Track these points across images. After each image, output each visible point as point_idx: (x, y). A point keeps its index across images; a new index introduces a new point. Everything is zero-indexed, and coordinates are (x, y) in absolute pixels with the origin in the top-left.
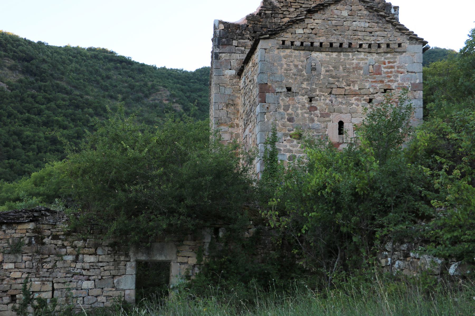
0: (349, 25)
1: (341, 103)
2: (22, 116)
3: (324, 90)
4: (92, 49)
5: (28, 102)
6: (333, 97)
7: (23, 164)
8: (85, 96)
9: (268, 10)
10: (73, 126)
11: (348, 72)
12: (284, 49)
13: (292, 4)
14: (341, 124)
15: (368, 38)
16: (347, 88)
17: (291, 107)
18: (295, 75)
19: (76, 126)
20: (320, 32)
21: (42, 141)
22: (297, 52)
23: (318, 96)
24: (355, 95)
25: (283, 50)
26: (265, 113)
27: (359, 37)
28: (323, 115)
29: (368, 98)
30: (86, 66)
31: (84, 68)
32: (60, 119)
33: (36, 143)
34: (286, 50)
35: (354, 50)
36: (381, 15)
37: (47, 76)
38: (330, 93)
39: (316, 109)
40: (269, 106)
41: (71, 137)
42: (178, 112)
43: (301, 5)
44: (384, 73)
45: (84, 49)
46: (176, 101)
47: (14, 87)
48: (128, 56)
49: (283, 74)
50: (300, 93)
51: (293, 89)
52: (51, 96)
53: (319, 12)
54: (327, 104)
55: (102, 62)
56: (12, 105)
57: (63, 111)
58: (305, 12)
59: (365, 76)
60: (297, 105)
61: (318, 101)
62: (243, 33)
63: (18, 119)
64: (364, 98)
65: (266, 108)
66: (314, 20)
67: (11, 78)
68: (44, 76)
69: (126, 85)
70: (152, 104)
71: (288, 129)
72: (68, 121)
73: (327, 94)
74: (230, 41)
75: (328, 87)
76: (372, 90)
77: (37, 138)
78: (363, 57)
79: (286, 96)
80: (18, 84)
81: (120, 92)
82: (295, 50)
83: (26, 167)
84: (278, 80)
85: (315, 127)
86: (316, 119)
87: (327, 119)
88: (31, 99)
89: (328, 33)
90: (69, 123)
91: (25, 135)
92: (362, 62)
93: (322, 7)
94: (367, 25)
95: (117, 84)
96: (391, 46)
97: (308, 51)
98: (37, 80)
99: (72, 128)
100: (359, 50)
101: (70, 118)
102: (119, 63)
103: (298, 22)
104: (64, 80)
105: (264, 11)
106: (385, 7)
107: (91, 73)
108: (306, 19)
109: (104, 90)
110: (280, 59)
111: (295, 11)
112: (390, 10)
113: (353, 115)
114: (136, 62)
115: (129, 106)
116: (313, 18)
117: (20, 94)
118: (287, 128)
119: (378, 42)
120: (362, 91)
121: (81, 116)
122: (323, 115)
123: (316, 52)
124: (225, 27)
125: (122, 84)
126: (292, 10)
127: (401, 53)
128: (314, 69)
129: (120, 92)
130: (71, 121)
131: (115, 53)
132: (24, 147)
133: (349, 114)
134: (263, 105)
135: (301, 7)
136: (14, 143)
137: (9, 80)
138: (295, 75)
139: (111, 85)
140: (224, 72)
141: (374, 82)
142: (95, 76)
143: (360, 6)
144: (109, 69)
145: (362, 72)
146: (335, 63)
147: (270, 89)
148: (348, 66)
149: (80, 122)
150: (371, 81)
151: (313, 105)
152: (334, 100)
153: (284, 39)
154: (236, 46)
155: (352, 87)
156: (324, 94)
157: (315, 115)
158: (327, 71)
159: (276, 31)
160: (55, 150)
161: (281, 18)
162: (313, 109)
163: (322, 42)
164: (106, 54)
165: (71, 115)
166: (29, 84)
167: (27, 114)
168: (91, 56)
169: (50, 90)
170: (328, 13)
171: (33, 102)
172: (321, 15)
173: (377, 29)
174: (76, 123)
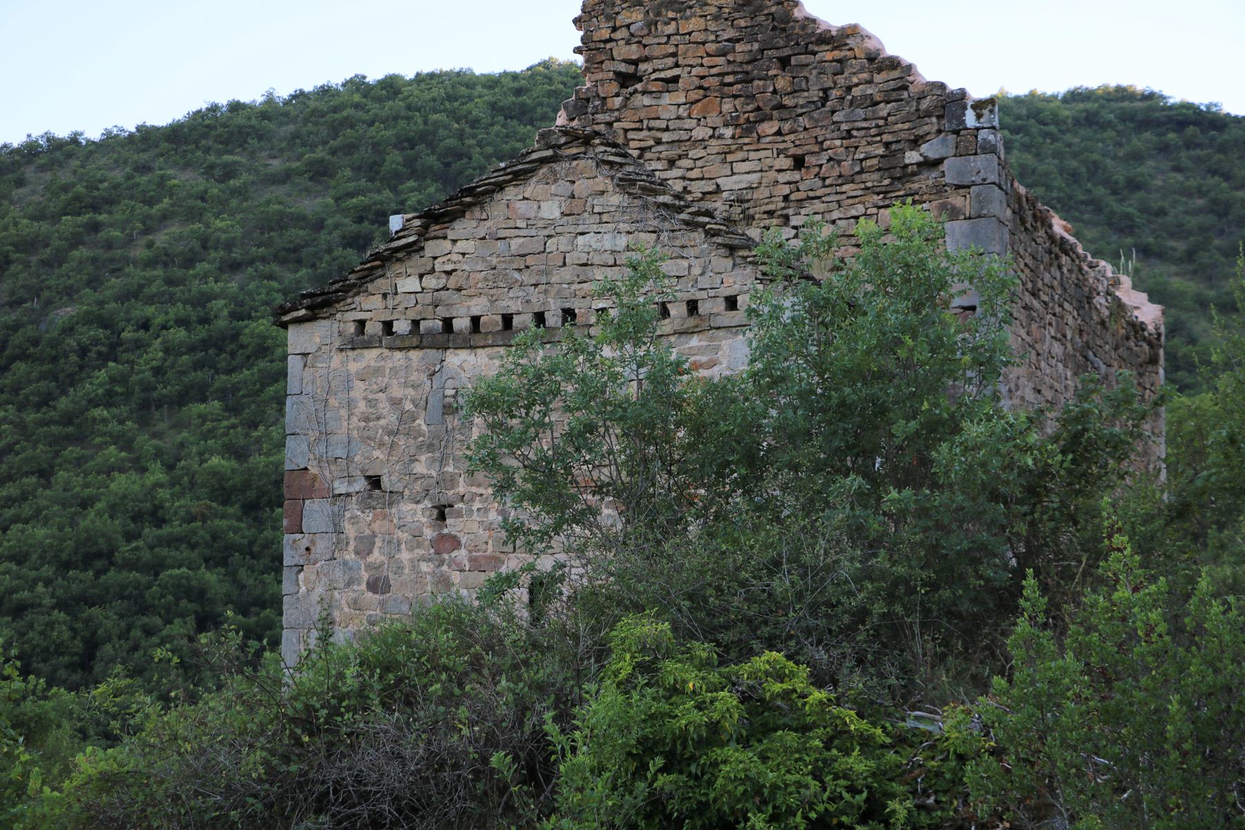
0: (562, 248)
4: (1080, 94)
12: (359, 351)
13: (631, 135)
17: (378, 543)
18: (390, 433)
22: (398, 355)
25: (356, 352)
30: (1057, 155)
31: (1050, 165)
34: (366, 352)
36: (666, 205)
39: (455, 543)
40: (313, 542)
43: (659, 135)
45: (1054, 97)
48: (1206, 102)
50: (407, 492)
53: (468, 214)
55: (1114, 133)
58: (417, 222)
61: (462, 516)
65: (303, 550)
66: (454, 241)
69: (1200, 202)
71: (370, 616)
79: (366, 506)
81: (1178, 231)
84: (340, 452)
93: (468, 199)
94: (622, 241)
95: (1166, 204)
96: (703, 309)
97: (434, 351)
102: (1174, 131)
103: (400, 255)
106: (943, 107)
107: (1074, 176)
108: (430, 243)
109: (1121, 231)
114: (1236, 117)
115: (1210, 278)
116: (451, 235)
123: (458, 351)
125: (1186, 203)
129: (1178, 231)
131: (1162, 97)
134: (294, 541)
135: (658, 142)
138: (390, 433)
139: (1144, 209)
142: (1089, 185)
143: (600, 178)
144: (1137, 157)
151: (446, 531)
153: (361, 316)
156: (481, 491)
157: (454, 567)
159: (328, 293)
162: (447, 545)
163: (478, 313)
164: (1126, 104)
168: (1074, 118)
170: (497, 209)
172: (474, 223)
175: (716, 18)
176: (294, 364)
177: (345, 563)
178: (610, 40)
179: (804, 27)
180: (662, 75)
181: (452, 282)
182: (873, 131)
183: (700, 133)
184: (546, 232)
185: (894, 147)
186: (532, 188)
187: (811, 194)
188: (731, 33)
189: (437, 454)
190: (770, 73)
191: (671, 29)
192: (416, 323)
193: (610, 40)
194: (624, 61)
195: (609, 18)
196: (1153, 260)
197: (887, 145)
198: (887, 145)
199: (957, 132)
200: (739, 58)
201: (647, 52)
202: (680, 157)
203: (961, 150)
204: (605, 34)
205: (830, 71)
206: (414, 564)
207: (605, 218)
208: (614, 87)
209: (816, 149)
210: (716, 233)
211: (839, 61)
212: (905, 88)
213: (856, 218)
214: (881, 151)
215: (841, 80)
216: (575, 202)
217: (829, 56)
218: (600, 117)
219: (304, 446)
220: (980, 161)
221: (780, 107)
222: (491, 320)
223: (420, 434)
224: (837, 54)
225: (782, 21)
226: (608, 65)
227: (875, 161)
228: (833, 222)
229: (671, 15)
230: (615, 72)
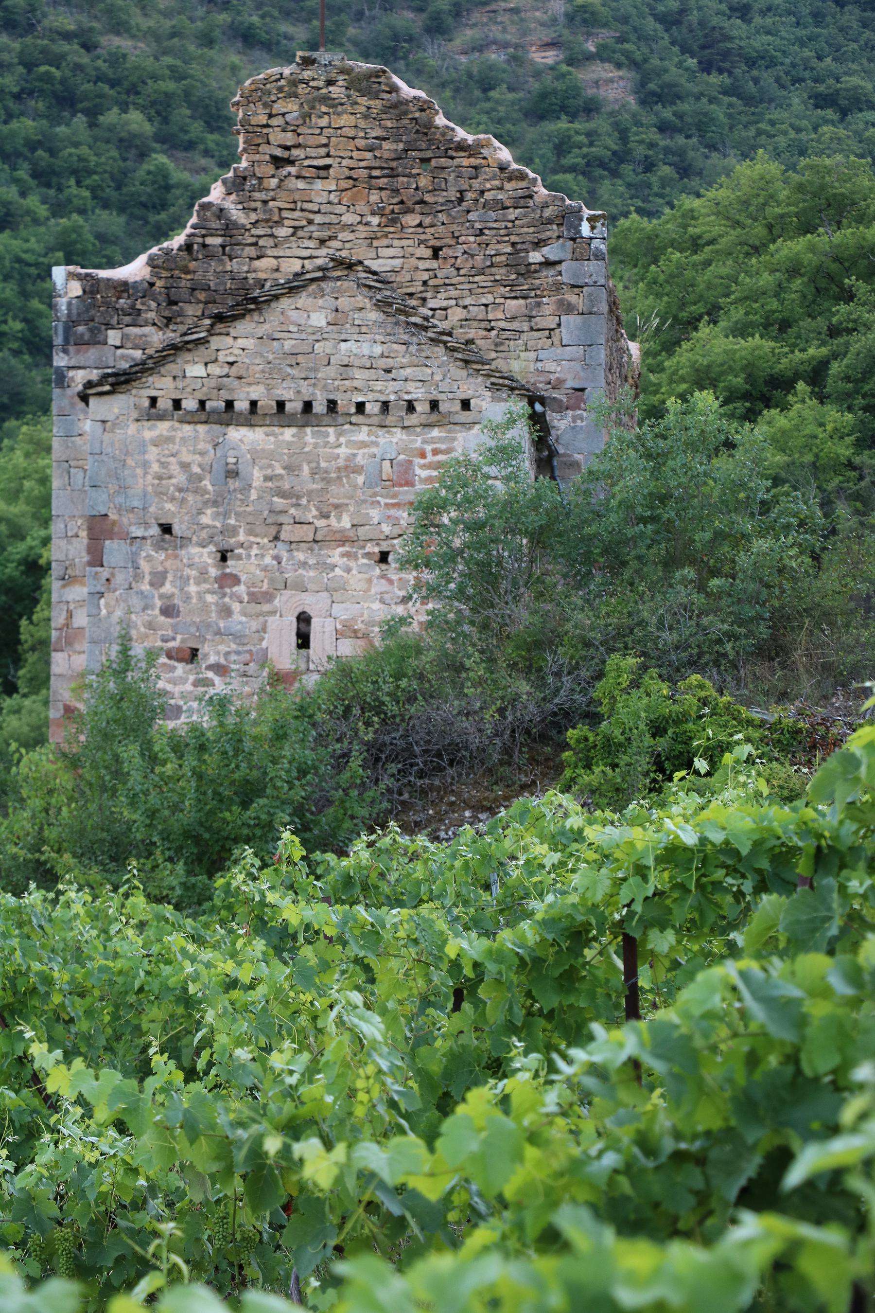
0: (328, 351)
1: (304, 564)
3: (258, 530)
6: (282, 550)
8: (104, 40)
9: (212, 235)
10: (43, 211)
11: (323, 479)
13: (285, 214)
14: (304, 619)
15: (379, 385)
17: (170, 577)
18: (180, 490)
19: (59, 209)
20: (251, 372)
22: (187, 428)
23: (242, 545)
24: (343, 542)
26: (101, 595)
27: (356, 383)
28: (255, 598)
29: (377, 550)
35: (340, 420)
36: (415, 325)
38: (276, 538)
39: (235, 580)
40: (113, 575)
41: (33, 271)
42: (611, 114)
43: (311, 216)
44: (422, 481)
46: (602, 47)
49: (150, 489)
50: (195, 538)
51: (176, 529)
53: (248, 317)
54: (265, 569)
59: (370, 492)
60: (187, 571)
62: (139, 306)
64: (367, 550)
70: (470, 75)
72: (17, 181)
73: (266, 540)
74: (99, 330)
75: (270, 521)
76: (386, 529)
78: (366, 438)
79: (159, 546)
82: (181, 422)
84: (136, 504)
85: (233, 631)
86: (236, 607)
87: (266, 607)
89: (272, 373)
90: (23, 194)
92: (361, 451)
96: (443, 407)
99: (36, 222)
100: (354, 419)
101: (26, 165)
103: (189, 346)
105: (200, 240)
110: (142, 447)
111: (293, 235)
113: (337, 596)
116: (233, 332)
118: (160, 633)
119: (407, 397)
120: (361, 531)
121: (84, 150)
122: (255, 598)
124: (84, 291)
126: (283, 232)
127: (468, 426)
128: (232, 473)
130: (33, 183)
133: (325, 594)
135: (310, 222)
138: (180, 490)
140: (81, 424)
141: (393, 505)
143: (360, 298)
145: (360, 479)
146: (290, 456)
147: (116, 529)
148: (323, 465)
149: (78, 183)
150: (386, 504)
151: (228, 571)
152: (285, 555)
153: (154, 393)
154: (117, 348)
155: (333, 521)
156: (258, 540)
158: (267, 478)
161: (251, 259)
162: (229, 582)
165: (33, 146)
172: (254, 325)
173: (404, 361)
174: (60, 190)
175: (365, 117)
177: (142, 593)
178: (267, 126)
179: (443, 134)
180: (315, 163)
181: (234, 371)
182: (502, 232)
183: (349, 218)
184: (315, 337)
185: (519, 247)
186: (303, 300)
187: (447, 281)
188: (378, 132)
189: (221, 510)
190: (414, 171)
191: (324, 122)
192: (202, 403)
193: (267, 126)
194: (280, 146)
195: (265, 105)
196: (257, 53)
197: (513, 244)
198: (513, 244)
199: (573, 239)
200: (386, 155)
201: (301, 140)
202: (330, 238)
203: (577, 255)
204: (263, 119)
205: (466, 175)
207: (364, 329)
208: (270, 170)
209: (453, 242)
210: (454, 350)
211: (475, 168)
212: (531, 197)
213: (486, 305)
214: (509, 249)
215: (476, 184)
216: (340, 315)
217: (465, 162)
218: (257, 195)
219: (105, 497)
221: (422, 202)
222: (267, 404)
223: (207, 492)
224: (473, 161)
225: (425, 127)
227: (503, 258)
228: (465, 307)
229: (324, 109)
230: (272, 156)
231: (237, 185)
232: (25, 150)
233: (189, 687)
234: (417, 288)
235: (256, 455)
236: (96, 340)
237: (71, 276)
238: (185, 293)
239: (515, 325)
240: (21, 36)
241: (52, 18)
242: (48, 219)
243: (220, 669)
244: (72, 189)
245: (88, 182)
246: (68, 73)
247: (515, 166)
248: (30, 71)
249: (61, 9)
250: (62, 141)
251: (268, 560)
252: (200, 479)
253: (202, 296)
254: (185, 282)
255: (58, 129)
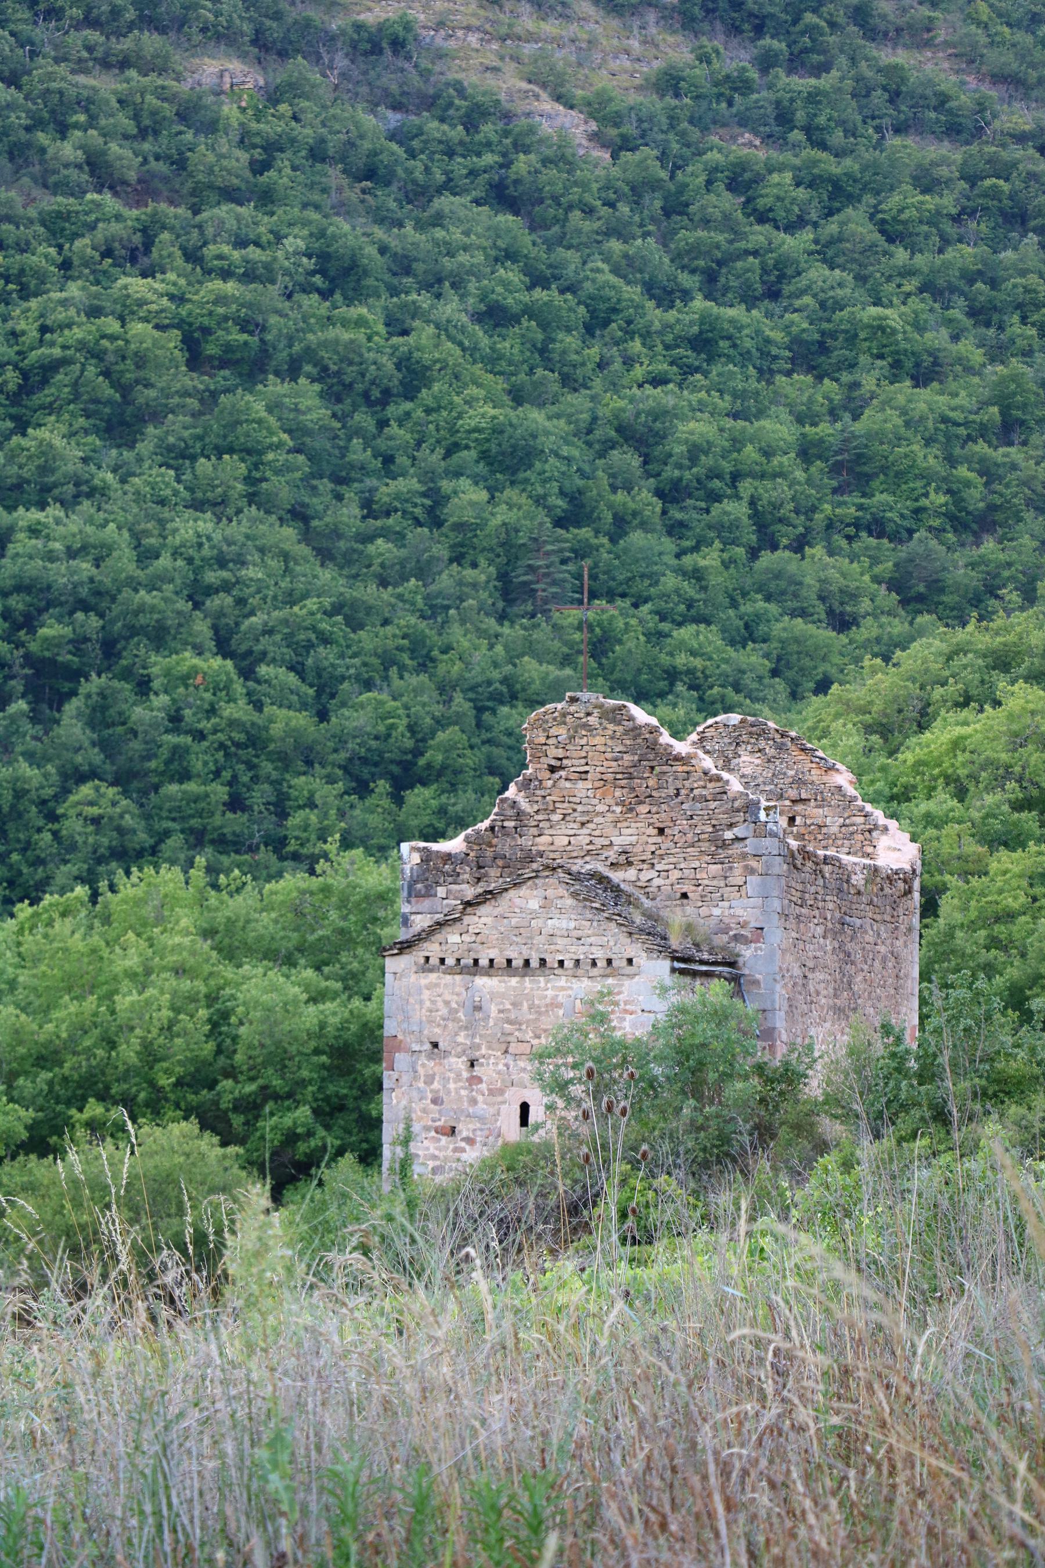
2: (672, 315)
5: (706, 222)
6: (510, 1060)
7: (665, 626)
10: (977, 356)
14: (525, 1108)
15: (573, 949)
16: (535, 1042)
19: (997, 353)
21: (781, 475)
28: (492, 1092)
32: (893, 316)
33: (746, 487)
37: (833, 25)
38: (506, 1052)
39: (480, 1080)
47: (630, 129)
52: (848, 162)
54: (499, 1073)
56: (615, 245)
57: (920, 260)
63: (646, 335)
67: (614, 65)
68: (811, 30)
77: (756, 456)
79: (430, 1057)
80: (655, 104)
83: (682, 646)
86: (480, 1098)
87: (500, 1099)
88: (728, 195)
91: (679, 442)
98: (766, 63)
99: (969, 370)
104: (941, 35)
112: (756, 815)
117: (664, 175)
121: (1033, 279)
122: (492, 1092)
126: (556, 817)
128: (478, 1008)
130: (968, 322)
132: (678, 515)
136: (620, 497)
137: (602, 81)
145: (561, 1012)
149: (1024, 320)
158: (500, 1011)
160: (857, 525)
166: (719, 96)
167: (699, 303)
169: (841, 123)
171: (739, 215)
174: (1001, 328)
176: (388, 977)
181: (479, 939)
183: (601, 808)
186: (524, 891)
191: (584, 741)
204: (542, 740)
206: (457, 1090)
208: (548, 774)
215: (687, 783)
217: (680, 769)
220: (767, 842)
226: (543, 760)
231: (526, 785)
232: (962, 284)
233: (449, 1153)
234: (648, 856)
235: (493, 996)
236: (429, 893)
237: (414, 849)
238: (488, 861)
239: (715, 883)
240: (968, 143)
241: (1004, 118)
242: (984, 365)
243: (470, 1141)
244: (1015, 327)
245: (1035, 317)
246: (1019, 185)
247: (714, 771)
248: (973, 185)
249: (1017, 105)
250: (1006, 269)
251: (501, 1067)
252: (457, 1011)
253: (500, 863)
254: (489, 853)
255: (1003, 255)
